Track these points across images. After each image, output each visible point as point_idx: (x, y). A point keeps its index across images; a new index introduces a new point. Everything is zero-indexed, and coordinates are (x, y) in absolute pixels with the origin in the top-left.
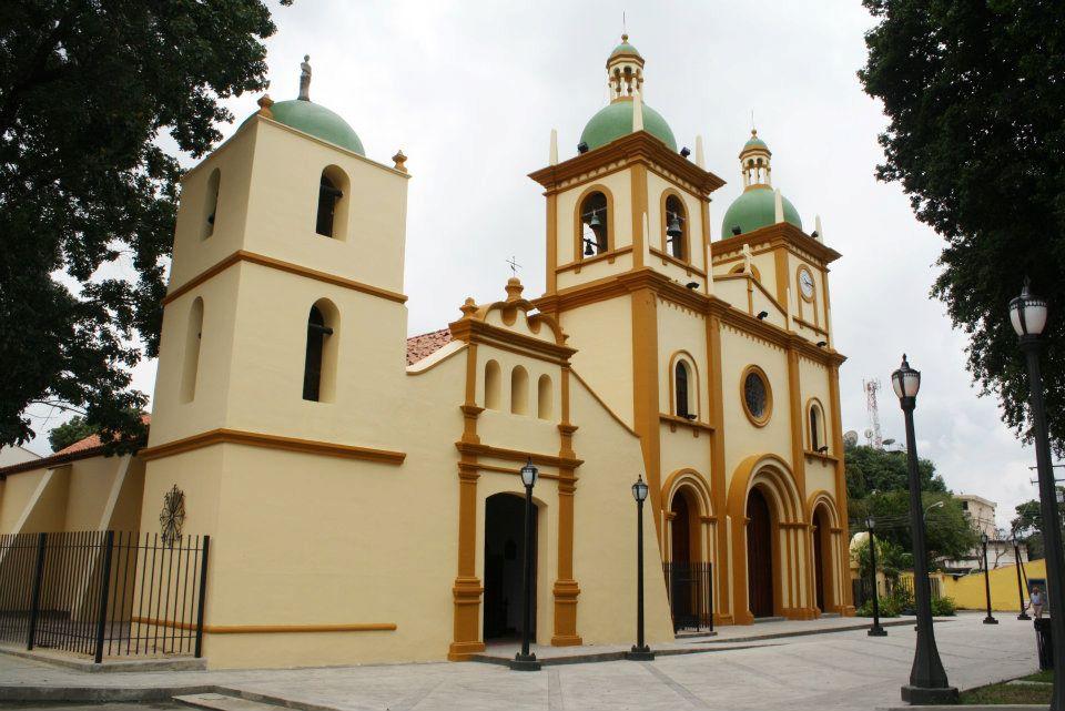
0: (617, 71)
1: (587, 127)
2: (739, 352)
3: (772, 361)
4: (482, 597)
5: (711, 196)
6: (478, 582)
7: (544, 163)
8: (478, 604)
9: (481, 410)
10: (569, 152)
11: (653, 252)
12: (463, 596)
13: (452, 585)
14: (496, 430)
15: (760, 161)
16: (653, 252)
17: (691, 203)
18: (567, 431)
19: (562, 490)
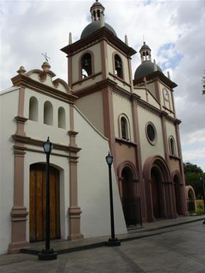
0: (94, 12)
1: (84, 31)
2: (145, 117)
3: (156, 121)
4: (28, 217)
5: (132, 57)
6: (26, 209)
7: (66, 44)
8: (25, 220)
9: (26, 120)
10: (77, 37)
11: (110, 74)
12: (16, 217)
13: (9, 210)
14: (35, 130)
15: (147, 52)
16: (110, 74)
17: (124, 59)
18: (72, 134)
19: (70, 162)
